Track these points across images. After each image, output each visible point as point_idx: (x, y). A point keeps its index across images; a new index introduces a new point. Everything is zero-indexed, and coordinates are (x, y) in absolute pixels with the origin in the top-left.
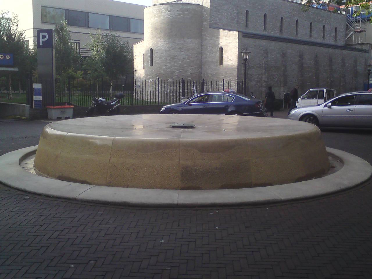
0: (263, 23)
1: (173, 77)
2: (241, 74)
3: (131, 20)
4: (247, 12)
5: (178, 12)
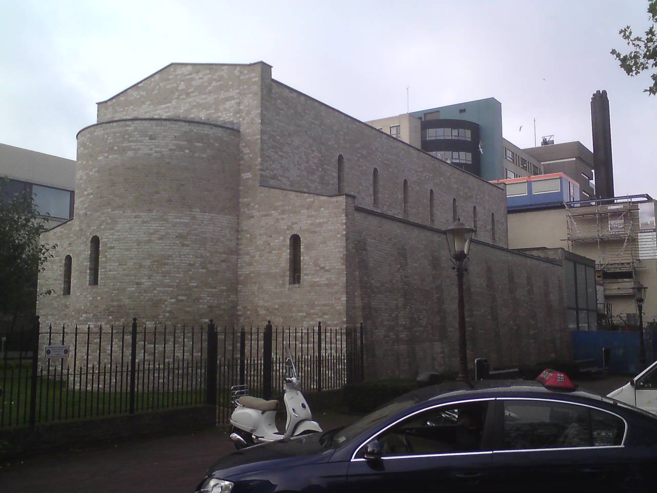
0: (371, 190)
1: (160, 315)
2: (354, 308)
3: (35, 189)
4: (340, 158)
5: (177, 142)
